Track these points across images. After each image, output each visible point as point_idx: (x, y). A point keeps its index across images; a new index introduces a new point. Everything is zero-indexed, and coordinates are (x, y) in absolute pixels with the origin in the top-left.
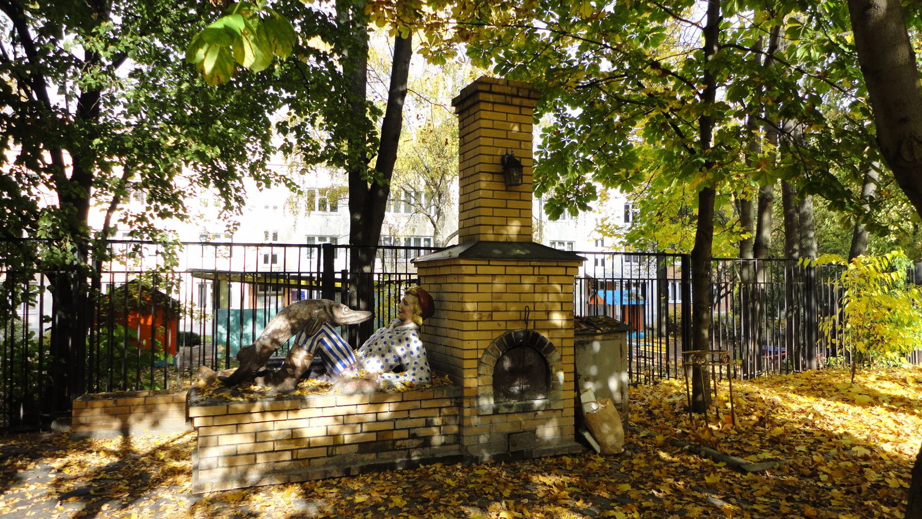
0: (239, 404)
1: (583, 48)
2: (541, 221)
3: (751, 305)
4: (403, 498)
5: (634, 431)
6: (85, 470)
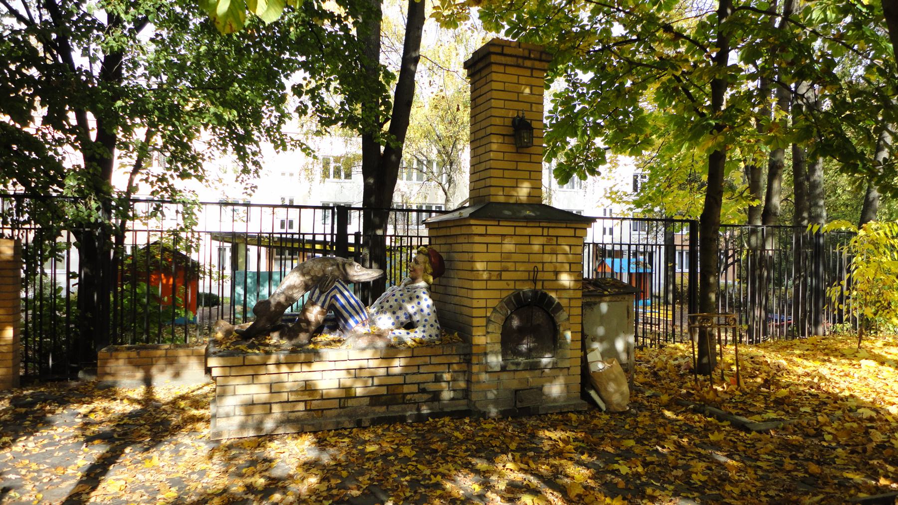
0: (255, 356)
1: (595, 12)
2: (550, 190)
3: (758, 272)
4: (412, 449)
5: (639, 391)
6: (109, 416)
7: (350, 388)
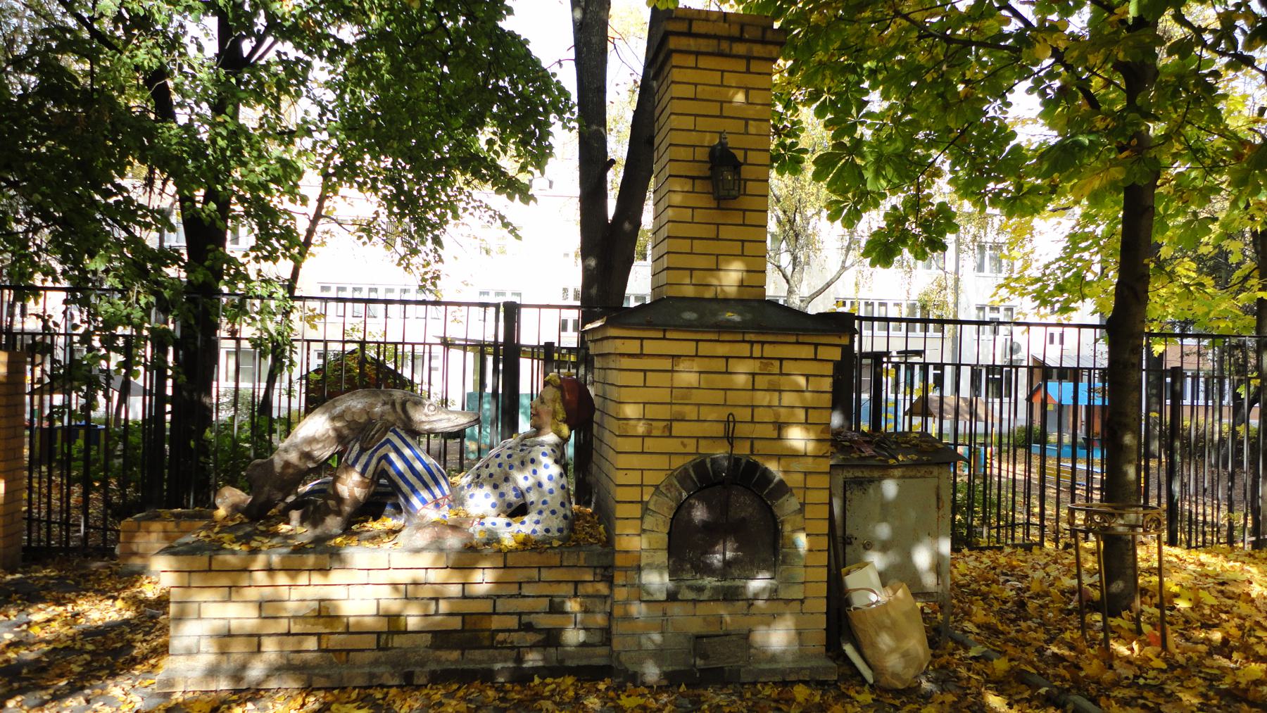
7: (398, 616)
